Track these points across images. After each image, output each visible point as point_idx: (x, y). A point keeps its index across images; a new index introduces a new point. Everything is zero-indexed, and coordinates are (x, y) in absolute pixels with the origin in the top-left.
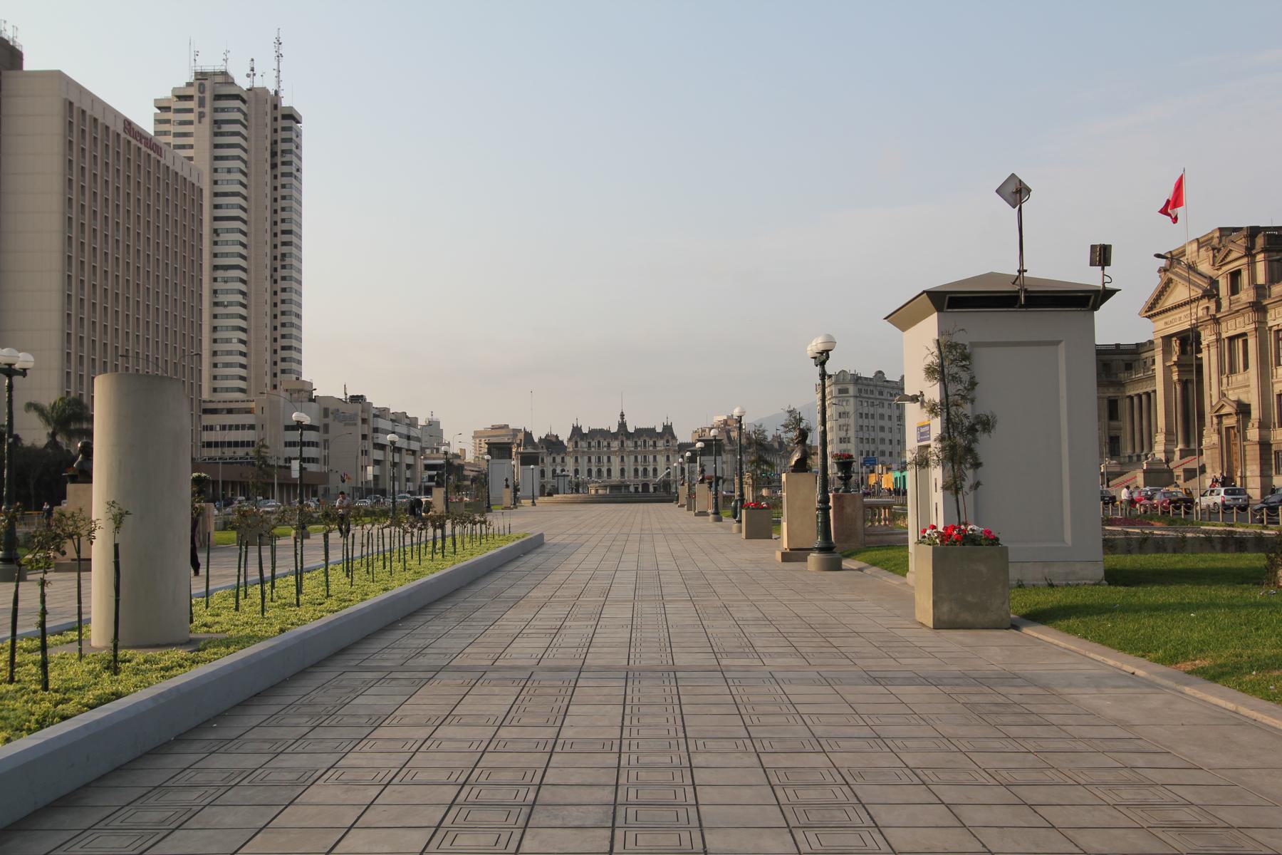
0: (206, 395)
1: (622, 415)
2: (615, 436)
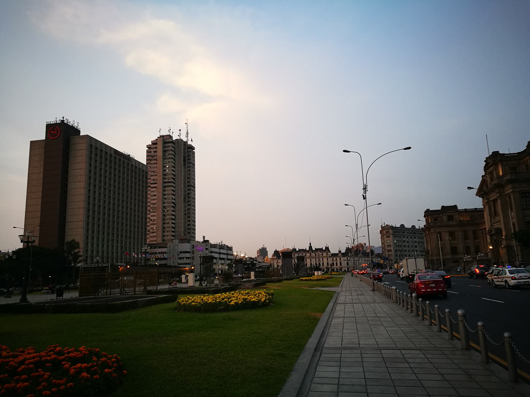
1: (310, 244)
2: (308, 251)
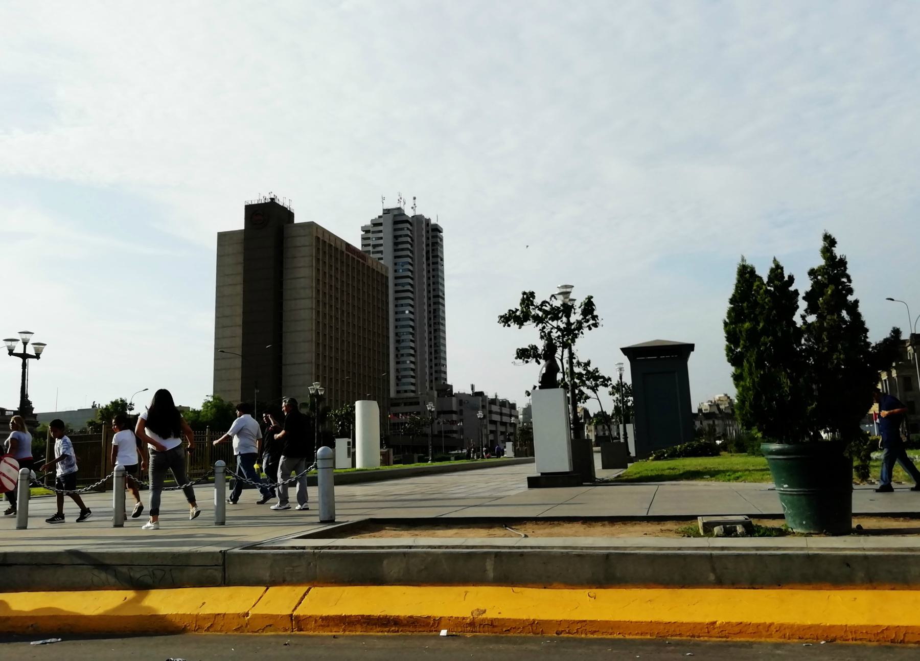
0: (393, 394)
